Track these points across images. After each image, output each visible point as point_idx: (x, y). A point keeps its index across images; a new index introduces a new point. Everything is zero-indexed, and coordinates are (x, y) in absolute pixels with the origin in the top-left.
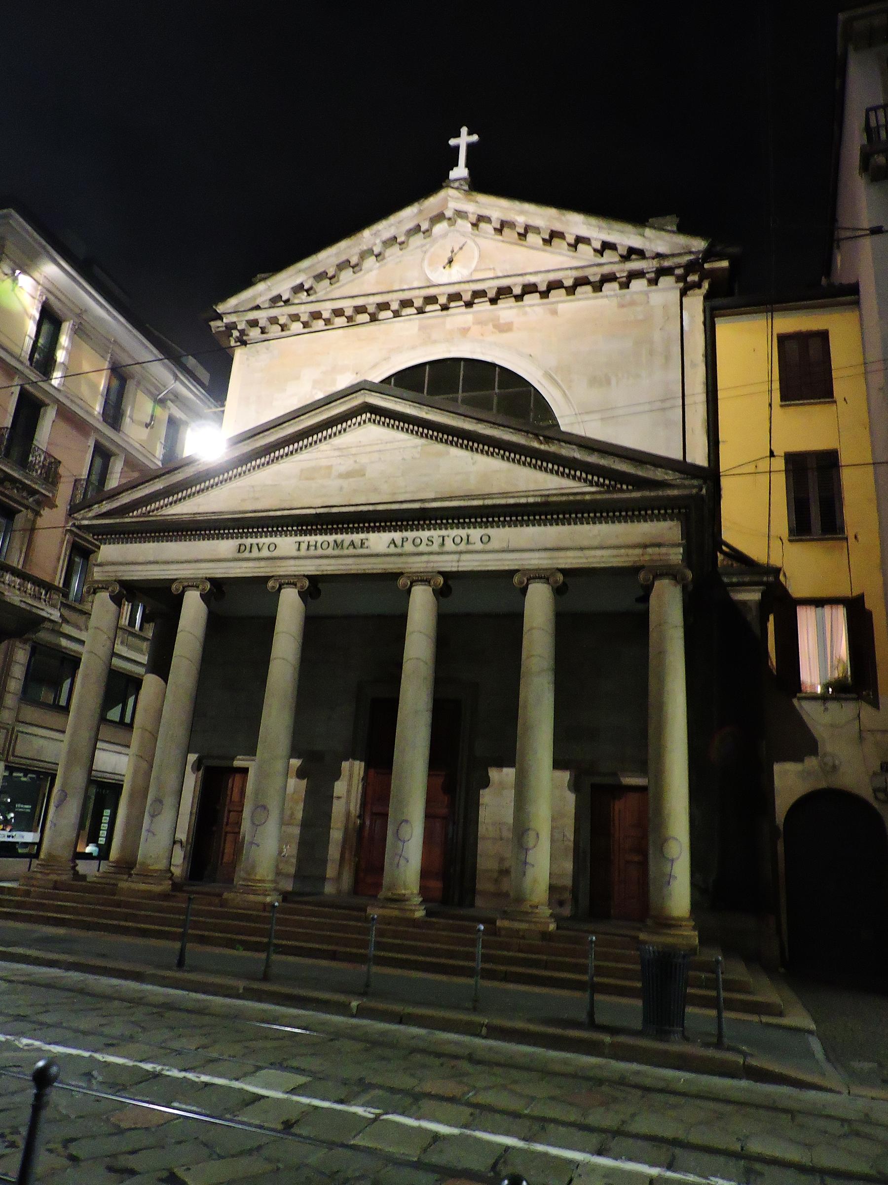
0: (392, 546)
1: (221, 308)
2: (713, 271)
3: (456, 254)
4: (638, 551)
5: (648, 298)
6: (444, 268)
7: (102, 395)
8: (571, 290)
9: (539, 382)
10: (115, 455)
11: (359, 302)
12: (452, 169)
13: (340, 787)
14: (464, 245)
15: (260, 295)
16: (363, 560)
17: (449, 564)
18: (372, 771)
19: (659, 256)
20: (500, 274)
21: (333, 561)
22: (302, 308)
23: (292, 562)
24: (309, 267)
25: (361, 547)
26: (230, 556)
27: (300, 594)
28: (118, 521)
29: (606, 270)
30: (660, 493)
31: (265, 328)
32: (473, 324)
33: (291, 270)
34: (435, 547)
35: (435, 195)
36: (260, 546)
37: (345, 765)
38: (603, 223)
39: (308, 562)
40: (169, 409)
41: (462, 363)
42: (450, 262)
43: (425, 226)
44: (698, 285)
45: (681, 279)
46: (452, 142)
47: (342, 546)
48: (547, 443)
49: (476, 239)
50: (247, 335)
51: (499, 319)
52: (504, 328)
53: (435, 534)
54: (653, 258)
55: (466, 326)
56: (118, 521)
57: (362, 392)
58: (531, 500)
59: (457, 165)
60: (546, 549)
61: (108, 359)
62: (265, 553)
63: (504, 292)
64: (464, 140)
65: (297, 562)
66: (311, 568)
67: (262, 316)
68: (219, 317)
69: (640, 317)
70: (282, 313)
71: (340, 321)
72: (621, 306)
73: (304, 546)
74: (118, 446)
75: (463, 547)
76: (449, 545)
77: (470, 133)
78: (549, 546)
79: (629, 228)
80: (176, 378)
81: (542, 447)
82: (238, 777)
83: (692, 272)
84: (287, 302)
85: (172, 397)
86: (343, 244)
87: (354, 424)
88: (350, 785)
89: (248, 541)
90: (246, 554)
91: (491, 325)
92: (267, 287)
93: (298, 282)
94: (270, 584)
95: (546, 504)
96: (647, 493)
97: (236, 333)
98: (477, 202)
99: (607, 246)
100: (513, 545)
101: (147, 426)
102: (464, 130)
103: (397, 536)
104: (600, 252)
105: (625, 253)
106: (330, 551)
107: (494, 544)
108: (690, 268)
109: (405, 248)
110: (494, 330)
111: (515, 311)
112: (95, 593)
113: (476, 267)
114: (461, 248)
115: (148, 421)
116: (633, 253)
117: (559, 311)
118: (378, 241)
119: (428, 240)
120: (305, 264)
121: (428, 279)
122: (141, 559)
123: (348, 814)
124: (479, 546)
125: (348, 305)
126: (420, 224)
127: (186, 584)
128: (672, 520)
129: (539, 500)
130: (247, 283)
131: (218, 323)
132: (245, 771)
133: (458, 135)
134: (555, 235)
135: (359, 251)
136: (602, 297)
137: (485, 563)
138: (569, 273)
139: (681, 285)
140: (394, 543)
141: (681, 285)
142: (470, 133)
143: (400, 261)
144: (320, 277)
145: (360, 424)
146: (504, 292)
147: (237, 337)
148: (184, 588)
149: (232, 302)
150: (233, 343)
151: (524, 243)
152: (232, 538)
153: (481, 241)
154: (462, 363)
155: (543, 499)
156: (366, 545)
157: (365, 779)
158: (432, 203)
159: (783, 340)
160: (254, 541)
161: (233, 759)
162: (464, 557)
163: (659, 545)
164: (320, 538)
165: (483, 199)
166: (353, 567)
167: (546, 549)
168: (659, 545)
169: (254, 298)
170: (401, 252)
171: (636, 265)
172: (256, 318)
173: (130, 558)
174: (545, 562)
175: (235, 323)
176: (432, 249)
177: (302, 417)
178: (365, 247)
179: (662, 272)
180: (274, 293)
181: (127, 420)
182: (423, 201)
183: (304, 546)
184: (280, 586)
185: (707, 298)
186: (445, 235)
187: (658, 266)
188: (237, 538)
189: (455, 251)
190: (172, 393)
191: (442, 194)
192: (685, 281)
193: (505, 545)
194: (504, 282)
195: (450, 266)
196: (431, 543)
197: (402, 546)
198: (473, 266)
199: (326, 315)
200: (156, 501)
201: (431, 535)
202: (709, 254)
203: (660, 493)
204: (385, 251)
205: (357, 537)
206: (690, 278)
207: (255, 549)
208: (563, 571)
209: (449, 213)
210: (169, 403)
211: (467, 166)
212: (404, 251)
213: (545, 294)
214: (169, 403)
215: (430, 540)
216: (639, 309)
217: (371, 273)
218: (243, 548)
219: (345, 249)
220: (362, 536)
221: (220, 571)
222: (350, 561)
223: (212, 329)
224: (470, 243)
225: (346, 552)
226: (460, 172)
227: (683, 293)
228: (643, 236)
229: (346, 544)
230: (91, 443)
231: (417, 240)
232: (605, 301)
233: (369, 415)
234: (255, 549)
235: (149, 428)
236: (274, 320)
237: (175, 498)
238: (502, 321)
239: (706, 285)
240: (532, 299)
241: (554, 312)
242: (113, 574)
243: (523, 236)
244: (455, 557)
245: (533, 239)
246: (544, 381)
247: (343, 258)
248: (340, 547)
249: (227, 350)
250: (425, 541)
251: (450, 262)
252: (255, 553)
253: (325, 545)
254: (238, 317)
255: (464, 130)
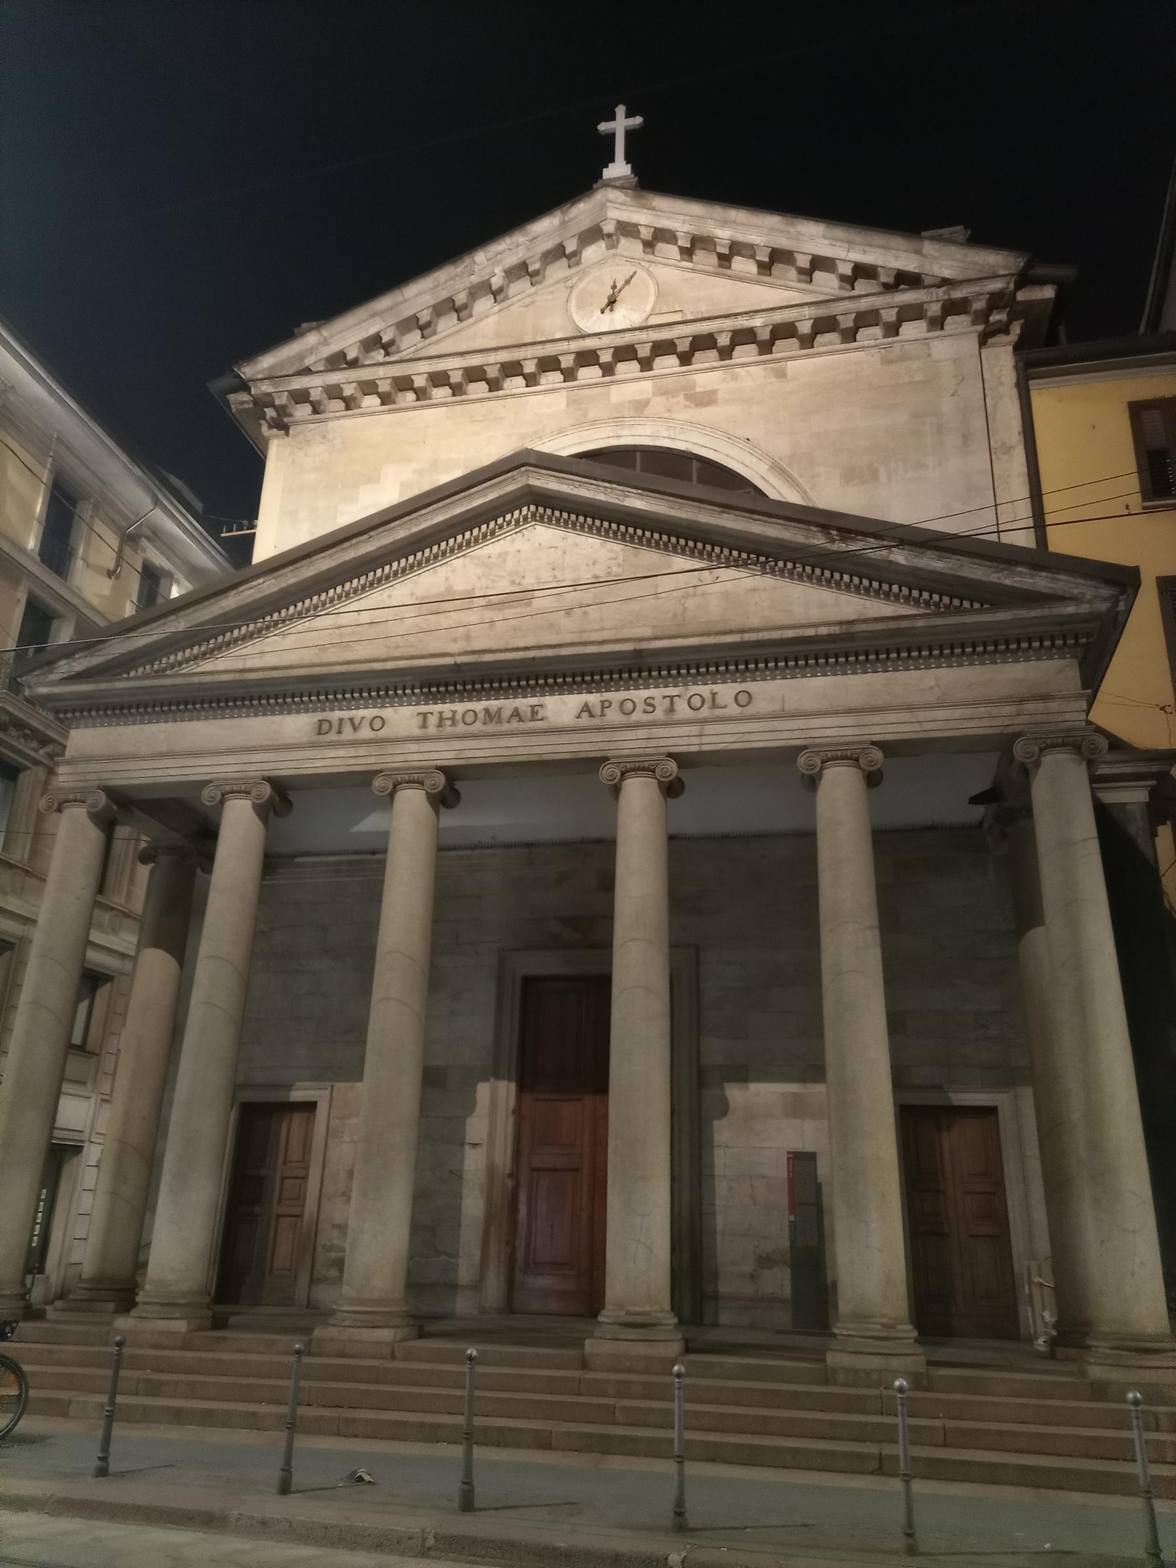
0: (585, 715)
1: (247, 371)
2: (1030, 305)
3: (620, 291)
4: (1010, 709)
5: (929, 348)
6: (603, 312)
7: (39, 521)
8: (807, 342)
9: (763, 478)
10: (59, 616)
11: (475, 361)
12: (607, 167)
13: (477, 1127)
14: (632, 277)
15: (311, 351)
16: (535, 740)
17: (685, 740)
18: (527, 1098)
19: (945, 282)
20: (690, 317)
21: (485, 743)
22: (381, 372)
23: (413, 747)
24: (390, 309)
25: (533, 719)
26: (304, 740)
27: (429, 796)
28: (103, 686)
29: (865, 304)
30: (1046, 612)
31: (319, 402)
32: (654, 394)
33: (361, 313)
34: (659, 715)
35: (586, 199)
36: (357, 722)
37: (483, 1091)
38: (854, 234)
39: (441, 746)
40: (144, 550)
41: (638, 454)
42: (612, 302)
43: (571, 247)
44: (1004, 329)
45: (982, 317)
46: (603, 127)
47: (499, 718)
48: (843, 540)
49: (651, 269)
50: (291, 415)
51: (694, 388)
52: (706, 399)
53: (656, 693)
54: (939, 287)
55: (644, 396)
56: (103, 686)
57: (523, 469)
58: (823, 631)
59: (613, 161)
60: (850, 711)
61: (49, 466)
62: (365, 733)
63: (703, 342)
64: (620, 124)
65: (425, 746)
66: (447, 753)
67: (315, 384)
68: (244, 386)
69: (919, 377)
70: (346, 379)
71: (442, 393)
72: (886, 361)
73: (433, 720)
74: (66, 602)
75: (705, 712)
76: (683, 710)
77: (629, 115)
78: (853, 705)
79: (898, 242)
80: (157, 502)
81: (843, 547)
82: (298, 1120)
83: (996, 309)
84: (354, 364)
85: (148, 533)
86: (442, 275)
87: (509, 524)
88: (493, 1124)
89: (336, 715)
90: (332, 737)
91: (682, 397)
92: (322, 339)
93: (372, 331)
94: (378, 782)
95: (850, 637)
96: (1023, 613)
97: (270, 413)
98: (654, 209)
99: (862, 271)
100: (791, 706)
101: (110, 574)
102: (621, 110)
103: (593, 699)
104: (848, 281)
105: (890, 280)
106: (478, 727)
107: (761, 706)
108: (996, 301)
109: (541, 282)
110: (688, 403)
111: (717, 374)
112: (59, 810)
113: (653, 309)
114: (627, 282)
115: (112, 567)
116: (905, 280)
117: (789, 373)
118: (498, 270)
119: (574, 270)
120: (383, 303)
121: (578, 328)
122: (144, 750)
123: (491, 1172)
124: (733, 710)
125: (454, 366)
126: (564, 244)
127: (228, 788)
128: (1062, 657)
129: (836, 630)
130: (284, 334)
131: (243, 397)
132: (311, 1106)
133: (612, 117)
134: (779, 257)
135: (468, 285)
136: (857, 349)
137: (746, 738)
138: (807, 312)
139: (980, 328)
140: (588, 711)
141: (980, 328)
142: (629, 115)
143: (532, 302)
144: (411, 324)
145: (517, 522)
146: (703, 342)
147: (272, 418)
148: (223, 795)
149: (267, 361)
150: (265, 428)
151: (728, 272)
152: (306, 711)
153: (661, 272)
154: (638, 454)
155: (844, 629)
156: (539, 716)
157: (518, 1111)
158: (581, 212)
159: (1137, 410)
160: (346, 714)
161: (289, 1087)
162: (709, 729)
163: (1045, 698)
164: (460, 707)
165: (662, 202)
166: (521, 751)
167: (850, 711)
168: (1045, 698)
169: (301, 357)
170: (533, 290)
171: (908, 297)
172: (305, 386)
173: (823, 306)
174: (850, 731)
175: (270, 394)
176: (582, 285)
177: (423, 512)
178: (475, 279)
179: (953, 308)
180: (334, 348)
181: (80, 564)
182: (570, 207)
183: (433, 720)
184: (395, 786)
185: (1018, 348)
186: (601, 263)
187: (946, 297)
188: (314, 711)
189: (619, 287)
190: (148, 527)
191: (599, 196)
192: (987, 321)
193: (777, 707)
194: (704, 328)
195: (611, 310)
196: (651, 709)
197: (603, 715)
198: (649, 308)
199: (419, 382)
200: (171, 653)
201: (651, 695)
202: (1024, 279)
203: (1046, 612)
204: (508, 286)
205: (524, 703)
206: (994, 318)
207: (347, 729)
208: (885, 747)
209: (609, 228)
210: (145, 543)
211: (628, 159)
212: (538, 287)
213: (766, 347)
214: (145, 543)
215: (649, 703)
216: (915, 365)
217: (486, 321)
218: (325, 726)
219: (446, 281)
220: (533, 701)
221: (286, 765)
222: (514, 742)
223: (232, 406)
224: (641, 274)
225: (506, 727)
226: (619, 169)
227: (983, 340)
228: (918, 252)
229: (506, 713)
230: (22, 596)
231: (558, 271)
232: (860, 355)
233: (533, 508)
234: (347, 729)
235: (113, 577)
236: (334, 392)
237: (203, 648)
238: (698, 390)
239: (1016, 329)
240: (746, 353)
241: (782, 375)
242: (94, 777)
243: (725, 260)
244: (695, 730)
245: (740, 264)
246: (771, 478)
247: (444, 294)
248: (496, 719)
249: (330, 368)
250: (641, 706)
251: (612, 302)
252: (348, 734)
253: (470, 718)
254: (274, 386)
255: (621, 110)
